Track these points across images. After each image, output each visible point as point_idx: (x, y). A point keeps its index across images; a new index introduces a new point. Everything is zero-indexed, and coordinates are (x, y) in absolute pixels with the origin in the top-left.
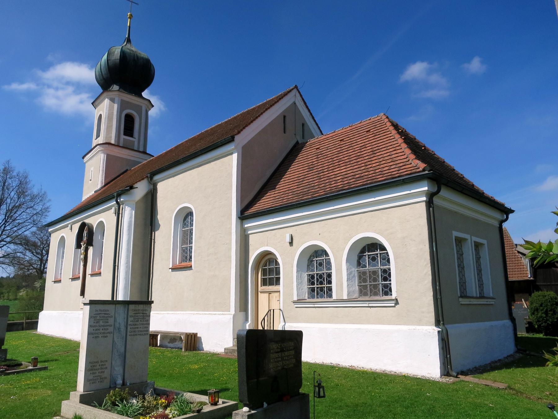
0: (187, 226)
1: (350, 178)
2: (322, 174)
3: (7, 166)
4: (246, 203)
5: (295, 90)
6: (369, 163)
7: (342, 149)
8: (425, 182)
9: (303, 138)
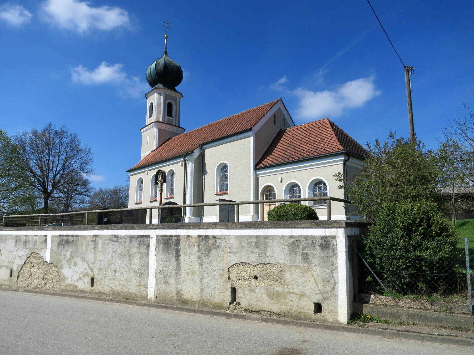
0: (224, 173)
1: (310, 152)
2: (296, 148)
3: (63, 129)
4: (257, 162)
5: (280, 102)
6: (319, 145)
7: (306, 135)
8: (343, 156)
9: (284, 126)
